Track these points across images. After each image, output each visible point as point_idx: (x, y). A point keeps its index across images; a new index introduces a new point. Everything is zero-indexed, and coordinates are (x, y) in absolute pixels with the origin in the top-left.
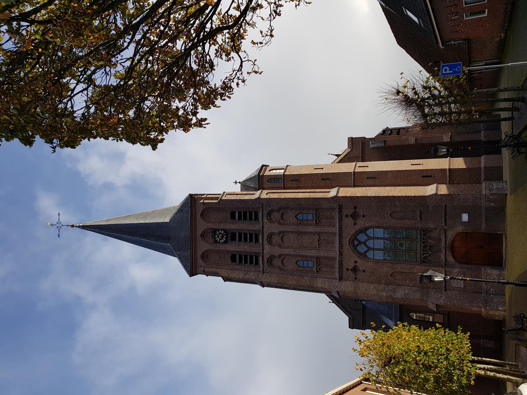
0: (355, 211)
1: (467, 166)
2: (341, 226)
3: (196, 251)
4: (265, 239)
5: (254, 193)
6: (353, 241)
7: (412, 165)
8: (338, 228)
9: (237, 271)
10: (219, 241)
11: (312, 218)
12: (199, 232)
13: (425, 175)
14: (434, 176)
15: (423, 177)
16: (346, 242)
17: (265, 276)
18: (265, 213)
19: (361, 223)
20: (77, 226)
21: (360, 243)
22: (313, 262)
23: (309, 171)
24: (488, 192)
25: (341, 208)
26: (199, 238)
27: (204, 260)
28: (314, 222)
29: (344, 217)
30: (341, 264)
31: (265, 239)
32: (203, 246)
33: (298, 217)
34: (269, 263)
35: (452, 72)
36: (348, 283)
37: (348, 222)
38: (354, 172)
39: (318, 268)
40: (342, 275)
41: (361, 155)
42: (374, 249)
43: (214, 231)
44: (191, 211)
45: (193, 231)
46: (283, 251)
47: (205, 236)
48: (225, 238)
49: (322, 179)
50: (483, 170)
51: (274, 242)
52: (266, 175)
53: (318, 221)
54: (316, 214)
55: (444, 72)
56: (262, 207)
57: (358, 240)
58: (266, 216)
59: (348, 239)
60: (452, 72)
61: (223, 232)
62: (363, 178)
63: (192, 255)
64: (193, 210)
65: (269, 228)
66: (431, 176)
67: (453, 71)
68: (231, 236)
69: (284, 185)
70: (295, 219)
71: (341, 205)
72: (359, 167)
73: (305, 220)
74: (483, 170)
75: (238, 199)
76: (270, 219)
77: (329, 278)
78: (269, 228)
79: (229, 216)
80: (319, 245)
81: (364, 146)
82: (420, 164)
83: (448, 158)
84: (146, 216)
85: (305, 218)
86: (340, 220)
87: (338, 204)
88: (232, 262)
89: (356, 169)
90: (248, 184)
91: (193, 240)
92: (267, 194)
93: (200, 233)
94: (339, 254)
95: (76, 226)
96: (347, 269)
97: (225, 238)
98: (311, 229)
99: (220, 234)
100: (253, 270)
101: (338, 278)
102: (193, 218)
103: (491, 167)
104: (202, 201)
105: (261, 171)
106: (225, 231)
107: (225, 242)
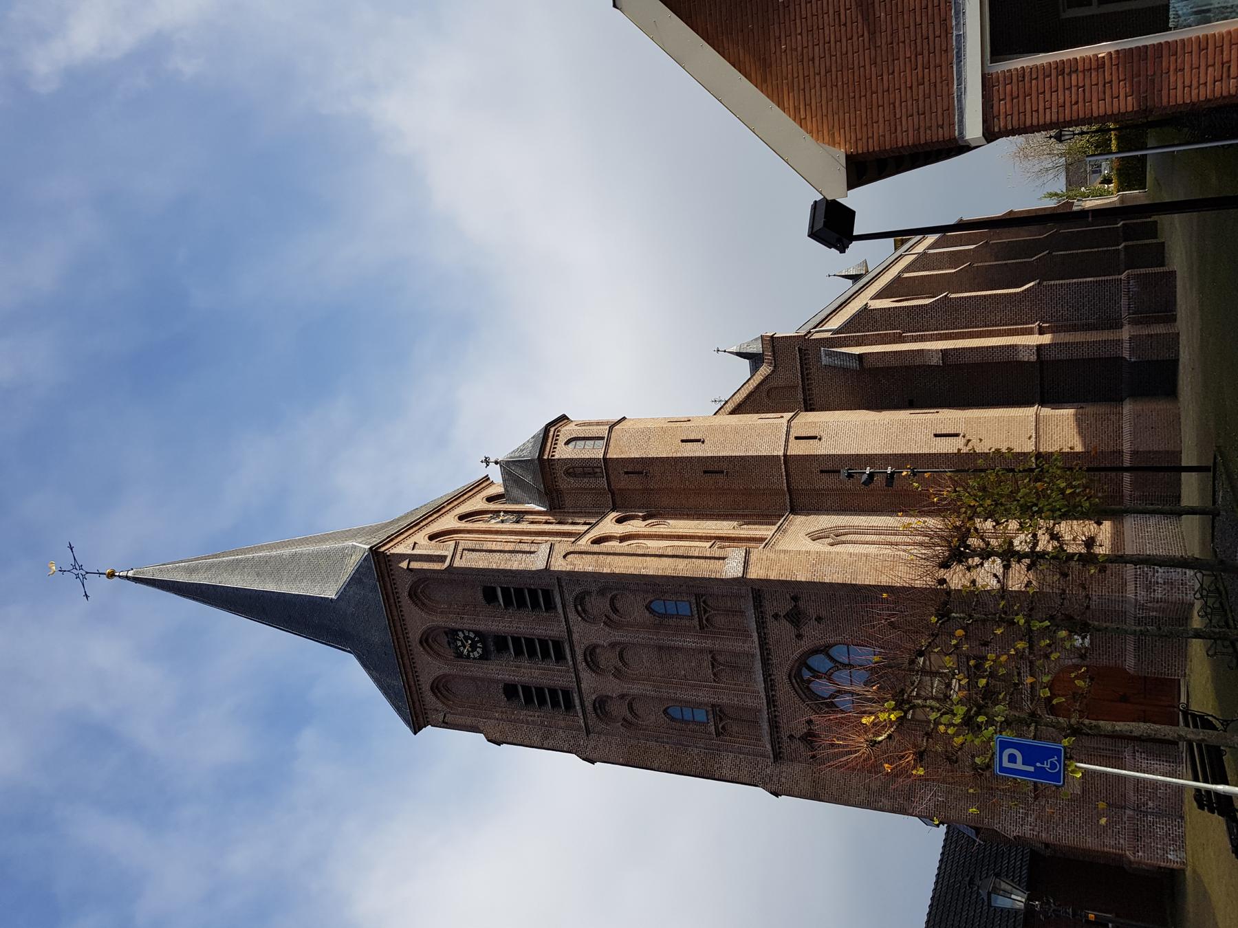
0: (795, 606)
1: (1084, 445)
2: (765, 639)
3: (417, 676)
4: (580, 658)
5: (532, 550)
6: (799, 671)
7: (936, 435)
8: (757, 643)
9: (525, 726)
10: (469, 655)
11: (689, 610)
12: (415, 635)
16: (781, 676)
17: (592, 744)
18: (570, 599)
19: (814, 635)
20: (122, 576)
21: (816, 674)
22: (707, 712)
23: (668, 449)
24: (1142, 593)
25: (760, 596)
26: (418, 649)
27: (439, 695)
28: (696, 622)
29: (769, 618)
30: (774, 726)
31: (580, 658)
32: (430, 668)
33: (652, 606)
34: (599, 711)
35: (1031, 769)
36: (798, 767)
37: (781, 630)
38: (785, 456)
39: (720, 726)
40: (780, 748)
41: (800, 382)
42: (850, 666)
43: (452, 633)
44: (384, 587)
45: (399, 632)
47: (430, 640)
48: (479, 647)
49: (705, 472)
51: (603, 663)
52: (559, 459)
53: (704, 621)
54: (698, 605)
55: (1006, 764)
56: (560, 586)
57: (810, 669)
58: (572, 605)
59: (786, 669)
60: (1031, 769)
61: (472, 635)
62: (812, 472)
63: (410, 687)
64: (389, 585)
65: (585, 634)
67: (1036, 768)
68: (498, 645)
69: (609, 484)
70: (647, 614)
71: (759, 590)
72: (797, 438)
73: (672, 616)
75: (494, 567)
76: (584, 610)
77: (748, 754)
78: (585, 634)
79: (480, 596)
80: (715, 675)
81: (805, 359)
82: (957, 435)
83: (1036, 407)
84: (278, 570)
85: (671, 609)
86: (761, 625)
87: (749, 588)
88: (508, 700)
89: (790, 444)
90: (518, 472)
91: (405, 652)
92: (564, 557)
93: (418, 636)
94: (768, 703)
95: (119, 576)
96: (791, 737)
97: (479, 647)
98: (689, 642)
99: (466, 638)
100: (562, 724)
101: (772, 756)
102: (392, 601)
103: (1150, 452)
104: (404, 565)
105: (546, 444)
106: (477, 633)
107: (481, 657)
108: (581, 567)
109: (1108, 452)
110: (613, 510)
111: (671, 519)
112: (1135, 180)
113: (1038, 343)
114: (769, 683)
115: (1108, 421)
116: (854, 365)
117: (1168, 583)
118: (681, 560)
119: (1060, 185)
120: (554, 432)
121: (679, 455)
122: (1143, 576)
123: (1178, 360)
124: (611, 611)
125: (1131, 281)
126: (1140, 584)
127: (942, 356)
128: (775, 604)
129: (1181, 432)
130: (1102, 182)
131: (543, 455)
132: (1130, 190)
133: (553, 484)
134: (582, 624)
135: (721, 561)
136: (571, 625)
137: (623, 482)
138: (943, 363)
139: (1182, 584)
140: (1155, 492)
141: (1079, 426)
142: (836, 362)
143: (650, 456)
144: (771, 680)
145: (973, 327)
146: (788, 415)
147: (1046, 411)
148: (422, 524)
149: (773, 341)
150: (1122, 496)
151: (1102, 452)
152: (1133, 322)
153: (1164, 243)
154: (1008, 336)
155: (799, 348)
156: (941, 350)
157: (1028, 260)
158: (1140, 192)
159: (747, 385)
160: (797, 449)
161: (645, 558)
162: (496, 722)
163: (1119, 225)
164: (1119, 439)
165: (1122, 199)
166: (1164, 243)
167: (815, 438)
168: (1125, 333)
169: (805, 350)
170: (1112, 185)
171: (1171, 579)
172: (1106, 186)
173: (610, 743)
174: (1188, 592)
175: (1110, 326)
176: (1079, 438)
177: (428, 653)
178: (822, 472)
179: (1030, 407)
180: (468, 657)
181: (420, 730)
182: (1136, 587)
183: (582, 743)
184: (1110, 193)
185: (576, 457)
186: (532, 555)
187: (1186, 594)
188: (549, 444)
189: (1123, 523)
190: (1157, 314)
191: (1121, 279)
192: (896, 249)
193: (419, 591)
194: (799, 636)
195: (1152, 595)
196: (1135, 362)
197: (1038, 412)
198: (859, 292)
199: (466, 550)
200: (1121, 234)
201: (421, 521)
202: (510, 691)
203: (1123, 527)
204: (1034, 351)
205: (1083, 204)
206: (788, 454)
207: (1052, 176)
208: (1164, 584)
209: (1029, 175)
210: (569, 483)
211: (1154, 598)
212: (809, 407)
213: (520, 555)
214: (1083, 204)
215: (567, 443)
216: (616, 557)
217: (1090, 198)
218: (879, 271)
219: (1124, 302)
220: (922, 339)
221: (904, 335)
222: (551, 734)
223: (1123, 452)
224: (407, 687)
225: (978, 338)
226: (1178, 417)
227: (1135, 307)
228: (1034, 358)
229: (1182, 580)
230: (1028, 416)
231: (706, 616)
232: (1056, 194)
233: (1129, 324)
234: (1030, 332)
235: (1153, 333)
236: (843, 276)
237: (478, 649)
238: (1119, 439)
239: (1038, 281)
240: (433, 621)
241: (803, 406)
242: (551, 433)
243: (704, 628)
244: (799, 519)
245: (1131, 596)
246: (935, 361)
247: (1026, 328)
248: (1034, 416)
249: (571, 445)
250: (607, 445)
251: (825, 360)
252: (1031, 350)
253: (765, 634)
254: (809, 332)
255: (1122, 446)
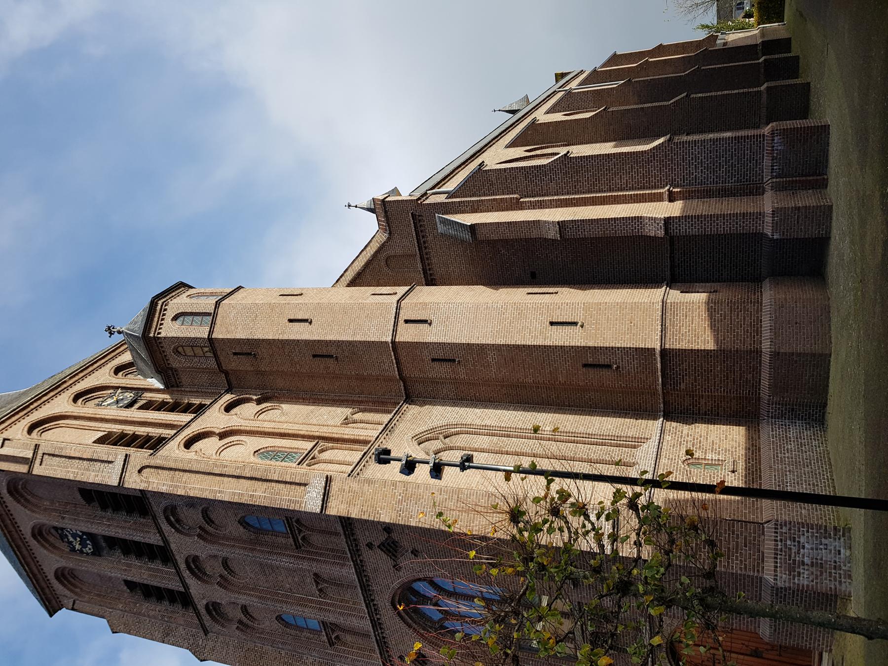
1: (717, 341)
2: (362, 566)
7: (552, 323)
13: (590, 361)
14: (618, 367)
15: (585, 366)
34: (214, 613)
37: (376, 560)
38: (393, 342)
46: (237, 598)
49: (314, 356)
50: (766, 359)
53: (300, 541)
62: (423, 361)
66: (609, 366)
70: (241, 528)
72: (406, 321)
74: (766, 359)
76: (178, 521)
81: (421, 226)
83: (664, 288)
92: (140, 471)
98: (285, 562)
105: (152, 320)
107: (93, 554)
108: (155, 486)
109: (744, 351)
110: (227, 392)
111: (287, 402)
112: (774, 14)
113: (666, 216)
114: (373, 608)
115: (745, 311)
116: (467, 236)
117: (817, 563)
118: (260, 483)
119: (711, 17)
120: (162, 306)
121: (285, 337)
122: (785, 552)
123: (830, 238)
124: (205, 522)
125: (776, 138)
126: (781, 563)
127: (560, 229)
128: (367, 533)
129: (830, 329)
130: (745, 17)
131: (149, 333)
132: (769, 23)
133: (165, 363)
134: (177, 535)
135: (302, 488)
136: (166, 535)
137: (233, 364)
138: (561, 237)
139: (835, 568)
140: (797, 399)
141: (711, 316)
142: (450, 231)
143: (256, 337)
144: (374, 605)
145: (597, 192)
146: (402, 290)
147: (675, 295)
148: (32, 407)
149: (384, 205)
150: (759, 398)
151: (737, 351)
152: (777, 188)
153: (809, 84)
154: (634, 202)
155: (412, 214)
156: (558, 222)
157: (665, 103)
158: (779, 25)
159: (365, 252)
160: (408, 334)
161: (222, 478)
162: (120, 612)
163: (760, 61)
164: (757, 335)
165: (763, 33)
166: (809, 84)
167: (425, 321)
168: (768, 203)
169: (419, 216)
170: (752, 19)
171: (821, 559)
172: (747, 19)
173: (228, 645)
174: (843, 580)
175: (750, 192)
176: (711, 332)
177: (43, 546)
178: (433, 360)
179: (658, 288)
180: (81, 552)
181: (55, 612)
182: (776, 567)
183: (200, 643)
184: (751, 26)
185: (182, 336)
186: (110, 465)
187: (840, 582)
188: (156, 319)
189: (759, 431)
190: (804, 178)
191: (764, 135)
192: (557, 81)
193: (20, 487)
194: (396, 567)
195: (796, 581)
196: (777, 239)
197: (665, 298)
198: (507, 131)
199: (46, 454)
200: (762, 70)
201: (32, 404)
202: (131, 585)
203: (759, 438)
204: (662, 225)
205: (726, 37)
206: (397, 340)
207: (702, 11)
208: (812, 566)
209: (682, 9)
210: (180, 362)
211: (798, 585)
212: (431, 281)
213: (99, 464)
214: (726, 37)
215: (175, 318)
216: (193, 475)
217: (733, 31)
218: (527, 111)
219: (767, 162)
220: (541, 205)
221: (522, 200)
222: (172, 631)
223: (761, 352)
224: (31, 576)
225: (601, 204)
226: (827, 310)
227: (779, 169)
228: (661, 233)
229: (835, 562)
230: (653, 303)
231: (302, 535)
232: (707, 27)
233: (772, 190)
234: (658, 198)
235: (800, 205)
236: (507, 111)
237: (89, 546)
238: (757, 335)
239: (668, 136)
240: (37, 518)
241: (422, 276)
242: (159, 307)
243: (300, 548)
244: (412, 411)
245: (769, 577)
246: (553, 234)
247: (654, 193)
248: (661, 304)
249: (179, 321)
250: (213, 323)
251: (441, 228)
252: (658, 224)
253: (361, 561)
254: (425, 194)
255: (761, 344)
